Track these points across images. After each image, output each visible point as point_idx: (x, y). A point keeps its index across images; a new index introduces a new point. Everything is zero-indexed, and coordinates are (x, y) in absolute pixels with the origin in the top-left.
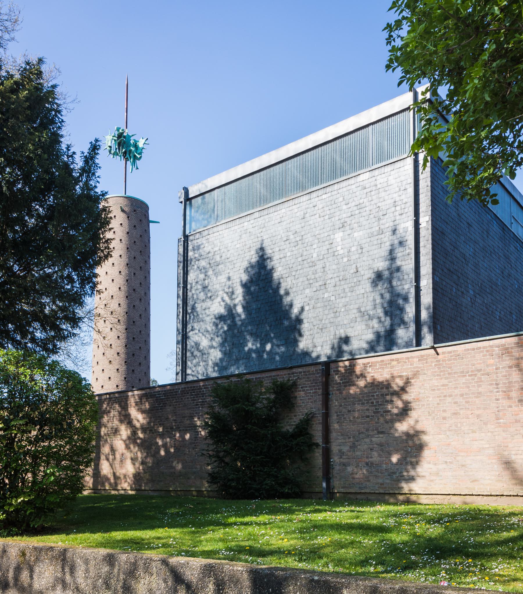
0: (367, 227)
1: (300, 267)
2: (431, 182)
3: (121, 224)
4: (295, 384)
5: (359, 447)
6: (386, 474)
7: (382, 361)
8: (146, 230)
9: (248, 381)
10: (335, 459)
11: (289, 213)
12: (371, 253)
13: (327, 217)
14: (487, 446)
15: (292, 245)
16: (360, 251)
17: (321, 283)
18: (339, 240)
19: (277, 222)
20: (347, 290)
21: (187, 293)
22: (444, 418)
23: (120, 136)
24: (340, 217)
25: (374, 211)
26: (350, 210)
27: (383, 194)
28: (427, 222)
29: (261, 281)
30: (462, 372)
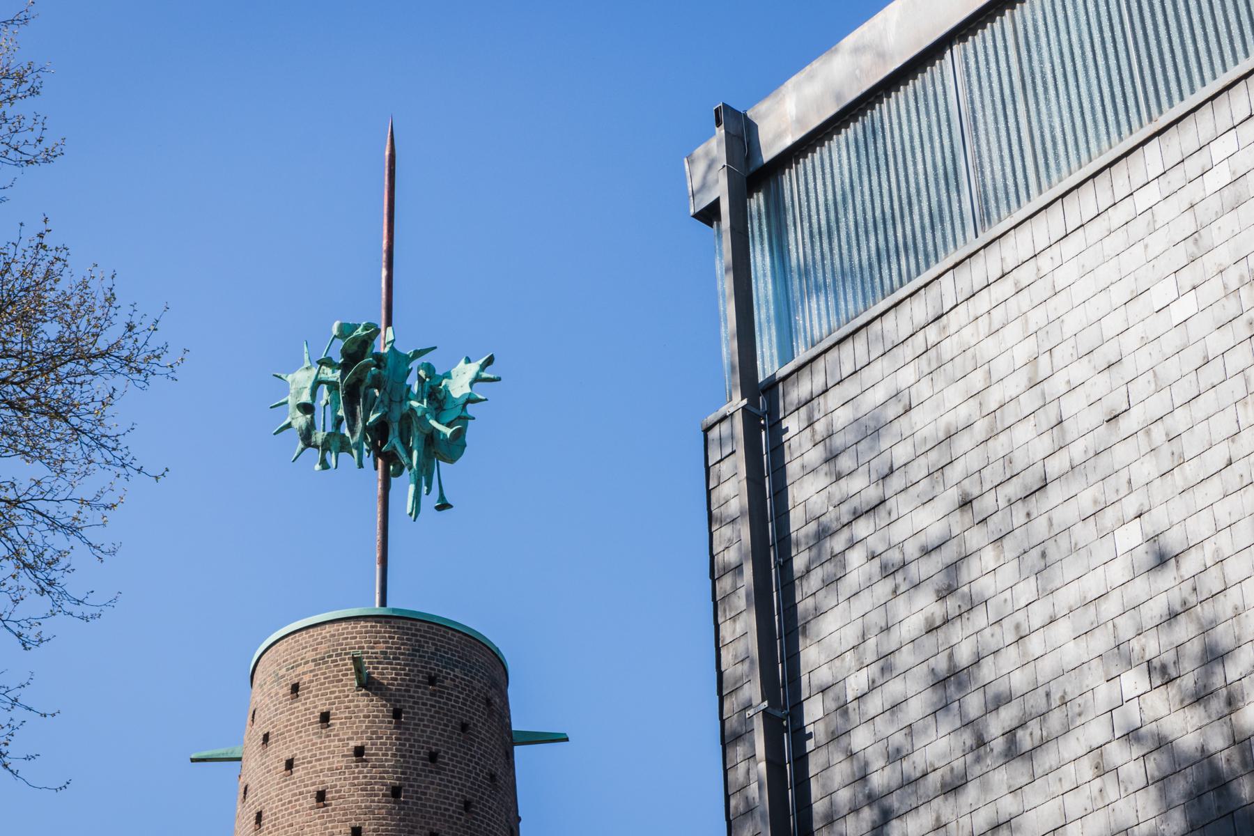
3: (359, 752)
8: (493, 777)
21: (801, 759)
23: (357, 351)
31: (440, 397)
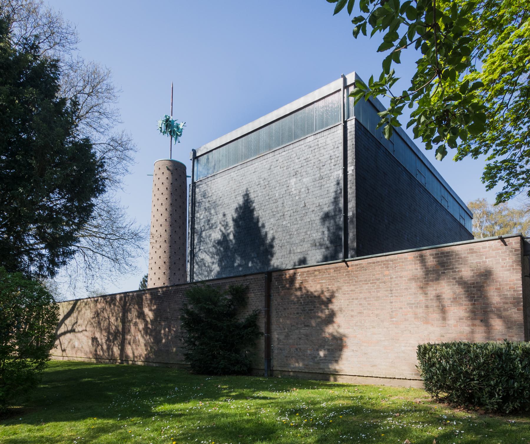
0: (312, 174)
1: (267, 203)
2: (356, 141)
4: (247, 288)
5: (291, 336)
6: (310, 358)
7: (308, 271)
9: (208, 286)
10: (275, 345)
11: (260, 166)
12: (314, 193)
13: (285, 168)
14: (383, 339)
15: (262, 188)
16: (307, 191)
17: (281, 214)
18: (293, 184)
19: (252, 172)
20: (298, 219)
22: (352, 316)
23: (167, 120)
24: (294, 168)
25: (316, 163)
26: (301, 163)
27: (323, 151)
28: (353, 170)
29: (246, 215)
30: (366, 281)
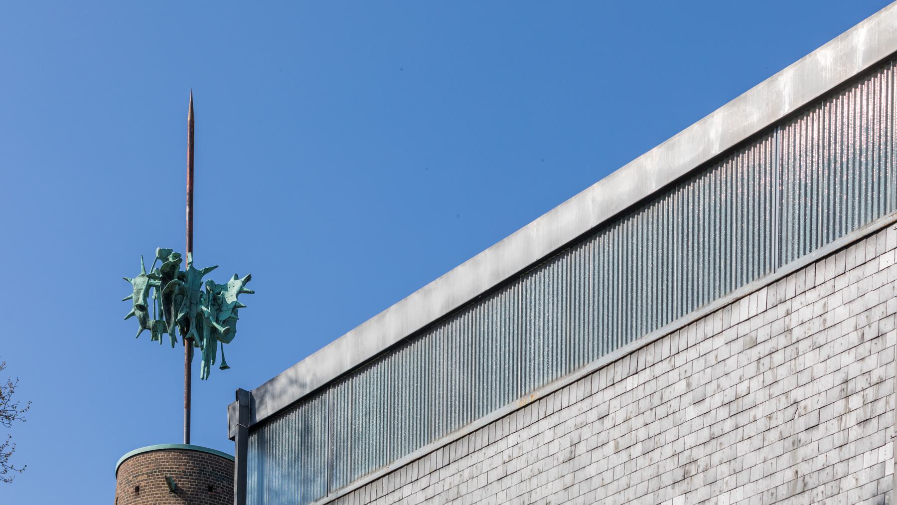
31: (220, 302)
